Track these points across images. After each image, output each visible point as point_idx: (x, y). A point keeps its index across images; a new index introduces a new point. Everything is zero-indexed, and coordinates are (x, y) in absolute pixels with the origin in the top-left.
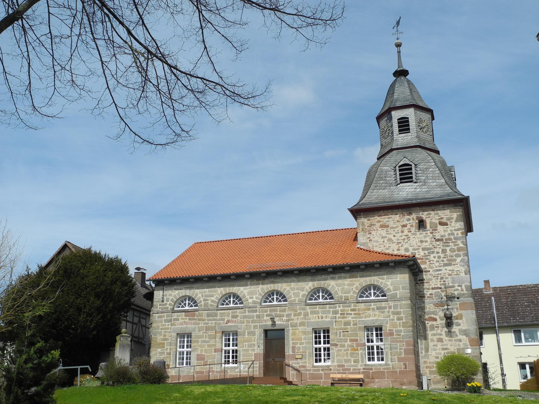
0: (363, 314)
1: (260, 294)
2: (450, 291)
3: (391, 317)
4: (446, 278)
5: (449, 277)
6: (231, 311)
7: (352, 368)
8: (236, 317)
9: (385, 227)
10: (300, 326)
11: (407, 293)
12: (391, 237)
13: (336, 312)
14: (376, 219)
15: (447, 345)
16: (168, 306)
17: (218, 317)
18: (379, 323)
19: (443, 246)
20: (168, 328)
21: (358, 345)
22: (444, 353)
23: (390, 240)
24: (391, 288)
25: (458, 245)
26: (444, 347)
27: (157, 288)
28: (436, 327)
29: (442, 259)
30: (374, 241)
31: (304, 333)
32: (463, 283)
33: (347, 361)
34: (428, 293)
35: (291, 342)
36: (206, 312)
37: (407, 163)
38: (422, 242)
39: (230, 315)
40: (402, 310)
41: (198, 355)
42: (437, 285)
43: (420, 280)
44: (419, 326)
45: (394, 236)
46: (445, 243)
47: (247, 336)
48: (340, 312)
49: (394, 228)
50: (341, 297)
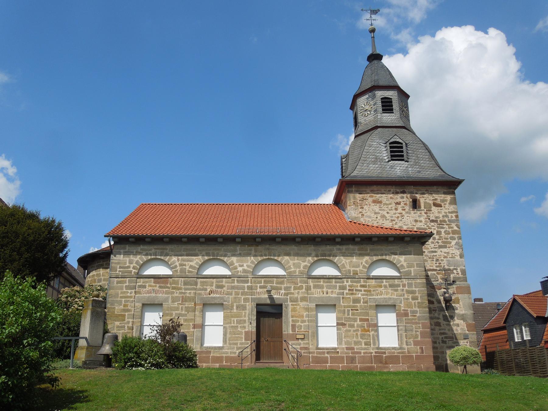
0: (373, 291)
3: (406, 296)
4: (442, 260)
5: (445, 259)
6: (215, 280)
7: (362, 351)
8: (222, 287)
9: (378, 203)
11: (422, 271)
12: (385, 213)
13: (343, 288)
15: (445, 330)
16: (131, 269)
17: (199, 286)
18: (392, 301)
19: (438, 227)
20: (131, 297)
21: (369, 326)
22: (442, 338)
23: (383, 216)
24: (405, 264)
25: (452, 228)
26: (442, 331)
27: (116, 246)
28: (434, 310)
29: (436, 241)
30: (367, 216)
31: (307, 309)
32: (458, 266)
33: (356, 343)
35: (291, 319)
36: (183, 279)
37: (398, 140)
38: (416, 221)
39: (214, 285)
40: (417, 289)
42: (432, 266)
45: (388, 213)
46: (439, 224)
47: (235, 311)
48: (348, 288)
49: (387, 205)
50: (349, 271)
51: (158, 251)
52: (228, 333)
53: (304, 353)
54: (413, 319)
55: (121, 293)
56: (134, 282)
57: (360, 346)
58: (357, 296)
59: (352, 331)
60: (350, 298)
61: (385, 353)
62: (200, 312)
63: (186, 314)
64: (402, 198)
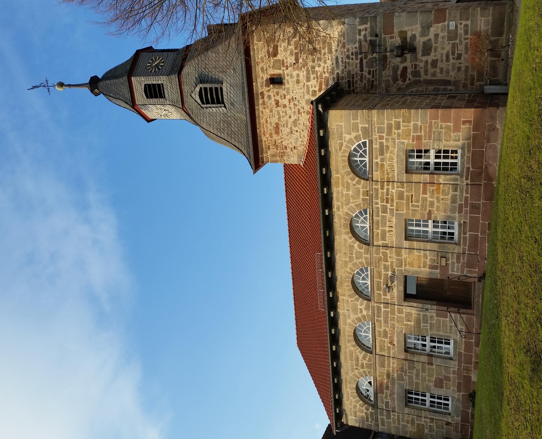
0: (388, 174)
1: (357, 300)
2: (366, 47)
4: (348, 51)
5: (347, 47)
7: (464, 195)
8: (385, 332)
10: (402, 256)
11: (363, 113)
14: (265, 139)
15: (442, 54)
18: (402, 154)
22: (453, 58)
23: (295, 123)
26: (444, 58)
28: (415, 68)
30: (296, 143)
34: (368, 76)
38: (298, 82)
39: (383, 339)
41: (435, 386)
42: (356, 64)
43: (349, 87)
44: (412, 91)
45: (290, 117)
48: (385, 204)
50: (363, 199)
51: (348, 386)
52: (438, 333)
53: (463, 259)
54: (425, 131)
55: (394, 423)
56: (383, 412)
57: (458, 197)
58: (394, 194)
59: (438, 204)
60: (397, 203)
61: (468, 169)
62: (414, 357)
63: (417, 370)
64: (269, 97)
